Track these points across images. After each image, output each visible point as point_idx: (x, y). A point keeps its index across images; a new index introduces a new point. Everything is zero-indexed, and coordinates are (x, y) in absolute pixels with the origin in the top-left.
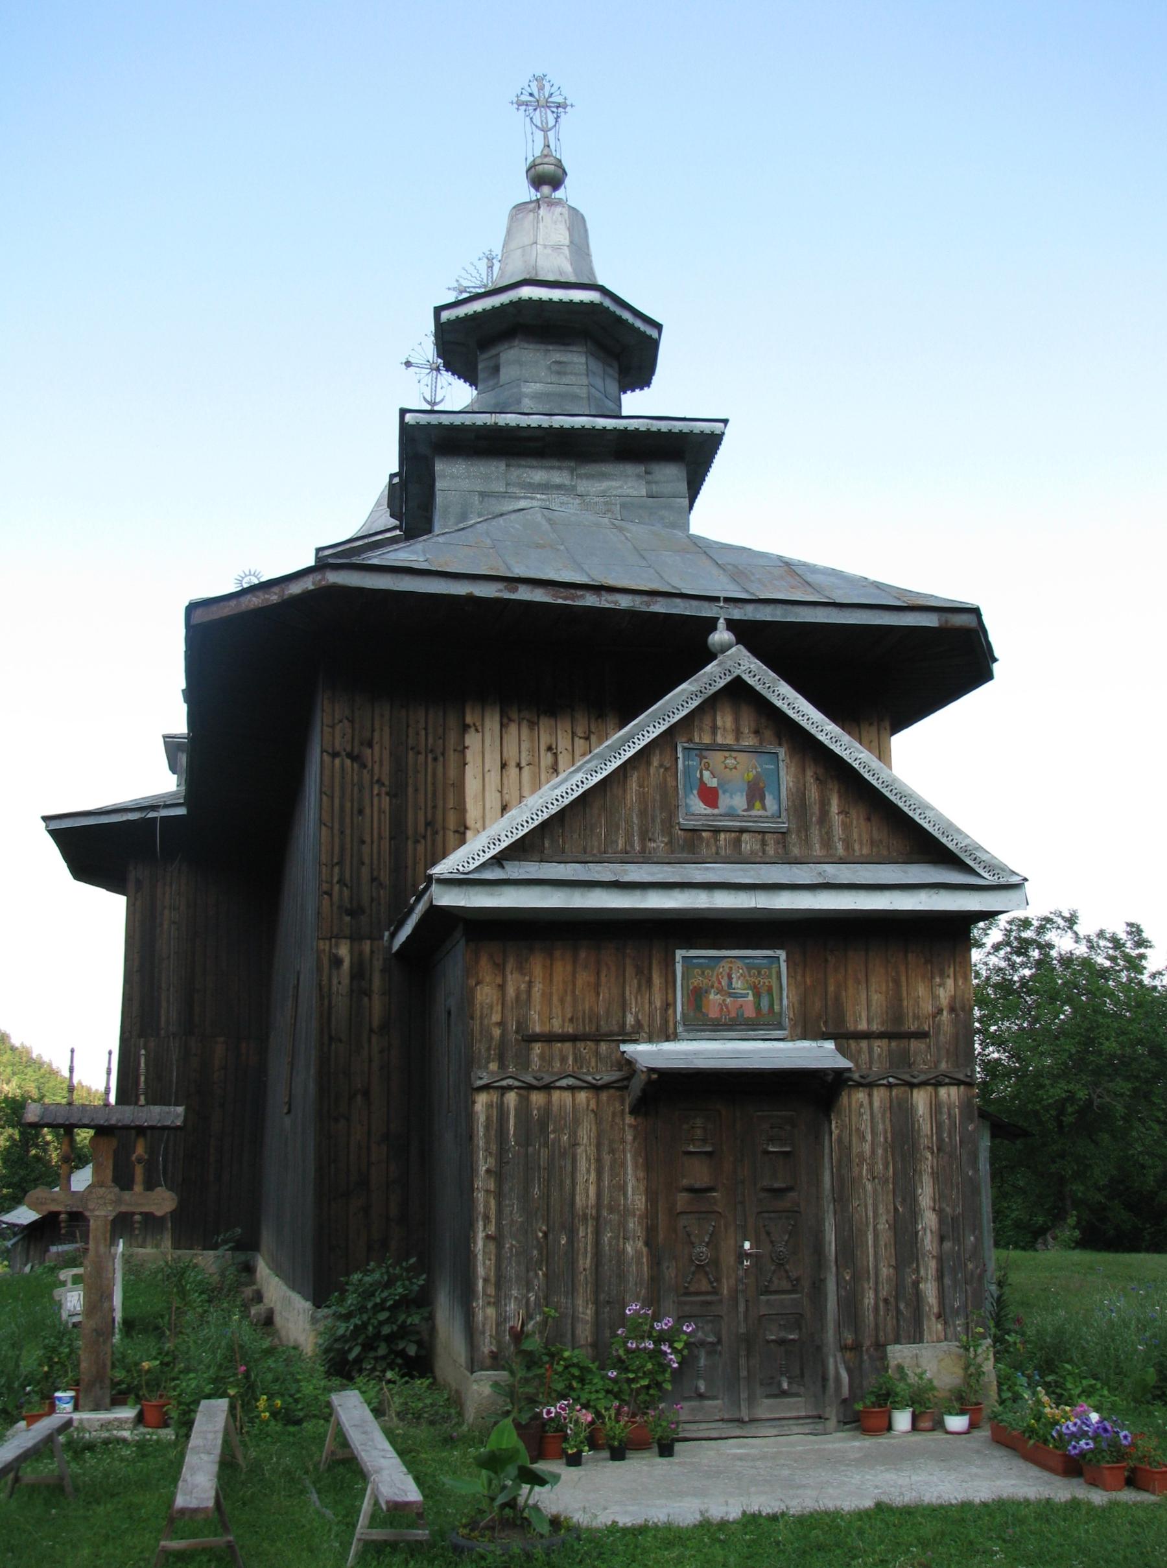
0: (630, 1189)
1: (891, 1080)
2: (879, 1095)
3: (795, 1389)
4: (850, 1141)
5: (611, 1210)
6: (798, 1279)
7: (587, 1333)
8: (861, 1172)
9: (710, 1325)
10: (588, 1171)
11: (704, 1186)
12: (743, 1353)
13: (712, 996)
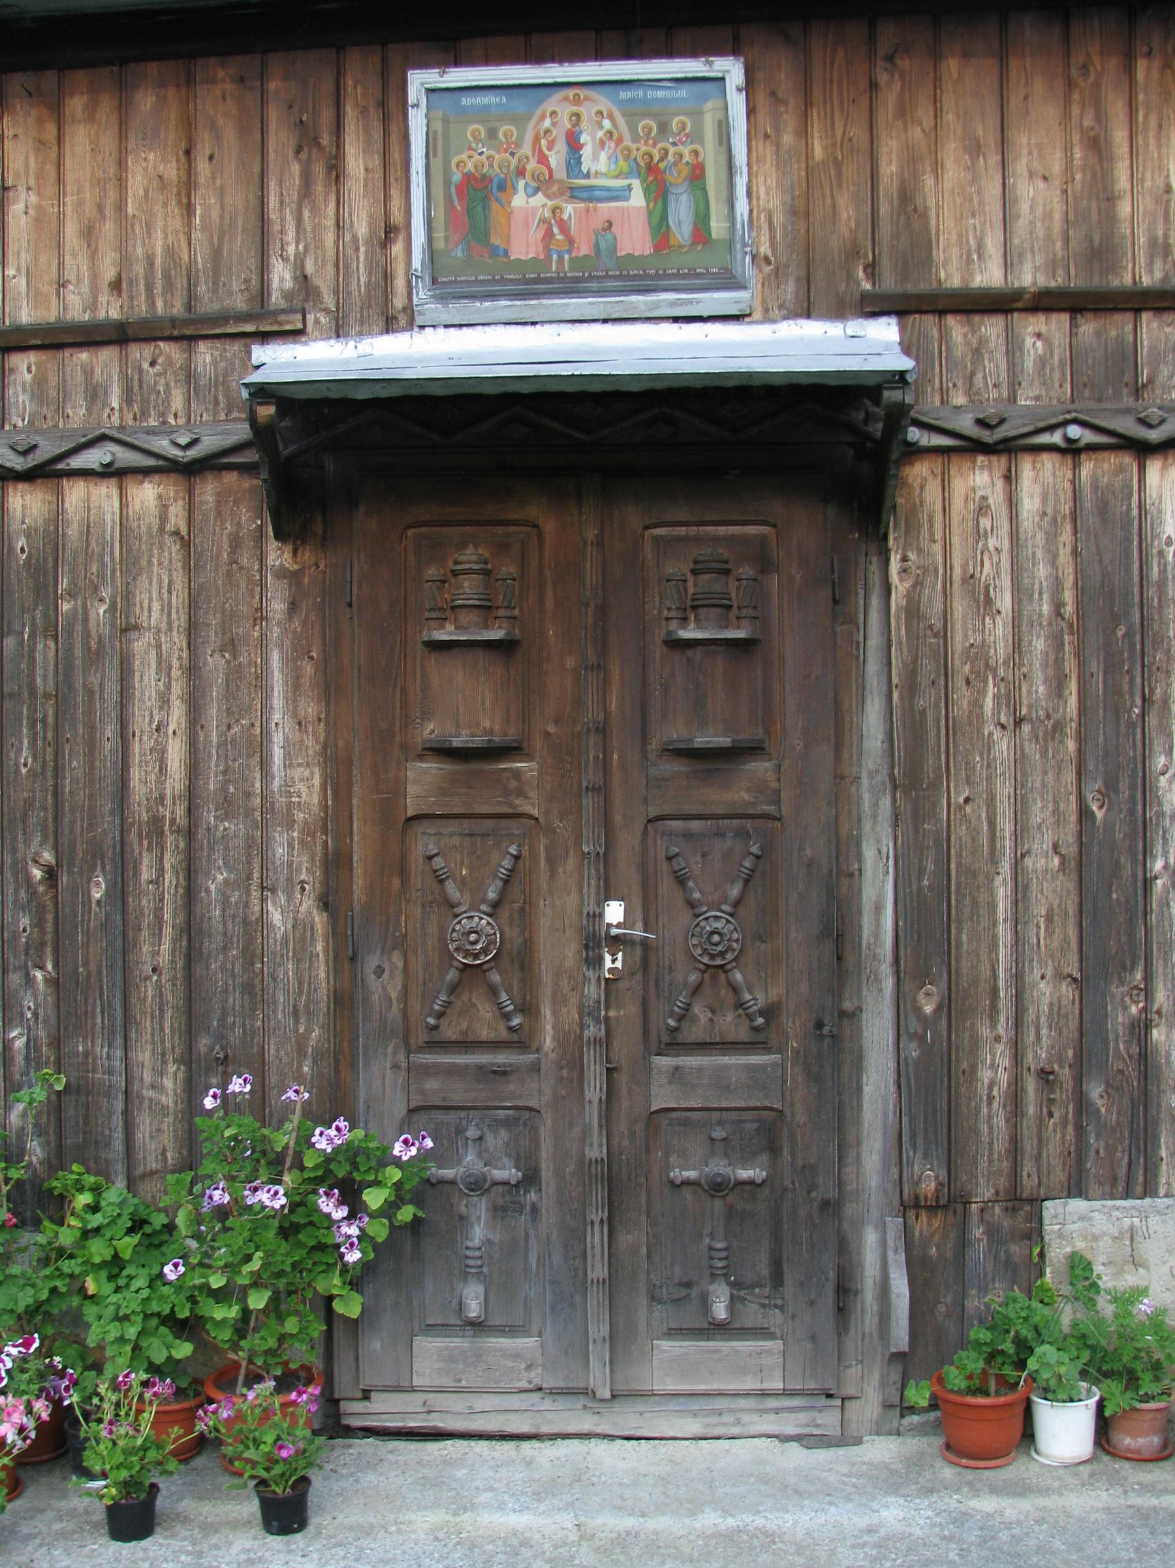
0: (278, 754)
1: (1074, 431)
2: (1039, 479)
3: (752, 1314)
4: (946, 614)
5: (227, 807)
6: (771, 1012)
7: (167, 1139)
8: (977, 703)
9: (504, 1133)
10: (164, 701)
11: (479, 741)
12: (597, 1214)
13: (519, 200)
